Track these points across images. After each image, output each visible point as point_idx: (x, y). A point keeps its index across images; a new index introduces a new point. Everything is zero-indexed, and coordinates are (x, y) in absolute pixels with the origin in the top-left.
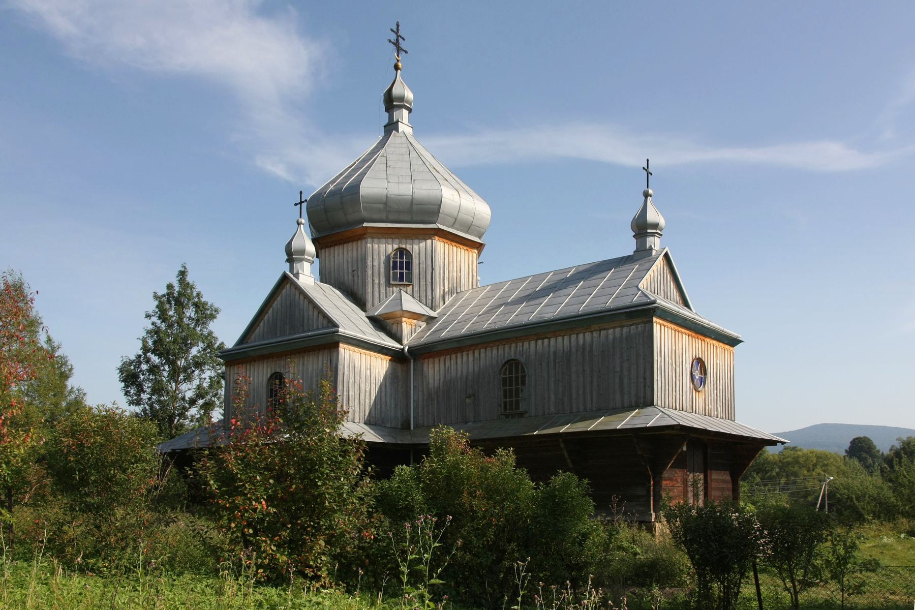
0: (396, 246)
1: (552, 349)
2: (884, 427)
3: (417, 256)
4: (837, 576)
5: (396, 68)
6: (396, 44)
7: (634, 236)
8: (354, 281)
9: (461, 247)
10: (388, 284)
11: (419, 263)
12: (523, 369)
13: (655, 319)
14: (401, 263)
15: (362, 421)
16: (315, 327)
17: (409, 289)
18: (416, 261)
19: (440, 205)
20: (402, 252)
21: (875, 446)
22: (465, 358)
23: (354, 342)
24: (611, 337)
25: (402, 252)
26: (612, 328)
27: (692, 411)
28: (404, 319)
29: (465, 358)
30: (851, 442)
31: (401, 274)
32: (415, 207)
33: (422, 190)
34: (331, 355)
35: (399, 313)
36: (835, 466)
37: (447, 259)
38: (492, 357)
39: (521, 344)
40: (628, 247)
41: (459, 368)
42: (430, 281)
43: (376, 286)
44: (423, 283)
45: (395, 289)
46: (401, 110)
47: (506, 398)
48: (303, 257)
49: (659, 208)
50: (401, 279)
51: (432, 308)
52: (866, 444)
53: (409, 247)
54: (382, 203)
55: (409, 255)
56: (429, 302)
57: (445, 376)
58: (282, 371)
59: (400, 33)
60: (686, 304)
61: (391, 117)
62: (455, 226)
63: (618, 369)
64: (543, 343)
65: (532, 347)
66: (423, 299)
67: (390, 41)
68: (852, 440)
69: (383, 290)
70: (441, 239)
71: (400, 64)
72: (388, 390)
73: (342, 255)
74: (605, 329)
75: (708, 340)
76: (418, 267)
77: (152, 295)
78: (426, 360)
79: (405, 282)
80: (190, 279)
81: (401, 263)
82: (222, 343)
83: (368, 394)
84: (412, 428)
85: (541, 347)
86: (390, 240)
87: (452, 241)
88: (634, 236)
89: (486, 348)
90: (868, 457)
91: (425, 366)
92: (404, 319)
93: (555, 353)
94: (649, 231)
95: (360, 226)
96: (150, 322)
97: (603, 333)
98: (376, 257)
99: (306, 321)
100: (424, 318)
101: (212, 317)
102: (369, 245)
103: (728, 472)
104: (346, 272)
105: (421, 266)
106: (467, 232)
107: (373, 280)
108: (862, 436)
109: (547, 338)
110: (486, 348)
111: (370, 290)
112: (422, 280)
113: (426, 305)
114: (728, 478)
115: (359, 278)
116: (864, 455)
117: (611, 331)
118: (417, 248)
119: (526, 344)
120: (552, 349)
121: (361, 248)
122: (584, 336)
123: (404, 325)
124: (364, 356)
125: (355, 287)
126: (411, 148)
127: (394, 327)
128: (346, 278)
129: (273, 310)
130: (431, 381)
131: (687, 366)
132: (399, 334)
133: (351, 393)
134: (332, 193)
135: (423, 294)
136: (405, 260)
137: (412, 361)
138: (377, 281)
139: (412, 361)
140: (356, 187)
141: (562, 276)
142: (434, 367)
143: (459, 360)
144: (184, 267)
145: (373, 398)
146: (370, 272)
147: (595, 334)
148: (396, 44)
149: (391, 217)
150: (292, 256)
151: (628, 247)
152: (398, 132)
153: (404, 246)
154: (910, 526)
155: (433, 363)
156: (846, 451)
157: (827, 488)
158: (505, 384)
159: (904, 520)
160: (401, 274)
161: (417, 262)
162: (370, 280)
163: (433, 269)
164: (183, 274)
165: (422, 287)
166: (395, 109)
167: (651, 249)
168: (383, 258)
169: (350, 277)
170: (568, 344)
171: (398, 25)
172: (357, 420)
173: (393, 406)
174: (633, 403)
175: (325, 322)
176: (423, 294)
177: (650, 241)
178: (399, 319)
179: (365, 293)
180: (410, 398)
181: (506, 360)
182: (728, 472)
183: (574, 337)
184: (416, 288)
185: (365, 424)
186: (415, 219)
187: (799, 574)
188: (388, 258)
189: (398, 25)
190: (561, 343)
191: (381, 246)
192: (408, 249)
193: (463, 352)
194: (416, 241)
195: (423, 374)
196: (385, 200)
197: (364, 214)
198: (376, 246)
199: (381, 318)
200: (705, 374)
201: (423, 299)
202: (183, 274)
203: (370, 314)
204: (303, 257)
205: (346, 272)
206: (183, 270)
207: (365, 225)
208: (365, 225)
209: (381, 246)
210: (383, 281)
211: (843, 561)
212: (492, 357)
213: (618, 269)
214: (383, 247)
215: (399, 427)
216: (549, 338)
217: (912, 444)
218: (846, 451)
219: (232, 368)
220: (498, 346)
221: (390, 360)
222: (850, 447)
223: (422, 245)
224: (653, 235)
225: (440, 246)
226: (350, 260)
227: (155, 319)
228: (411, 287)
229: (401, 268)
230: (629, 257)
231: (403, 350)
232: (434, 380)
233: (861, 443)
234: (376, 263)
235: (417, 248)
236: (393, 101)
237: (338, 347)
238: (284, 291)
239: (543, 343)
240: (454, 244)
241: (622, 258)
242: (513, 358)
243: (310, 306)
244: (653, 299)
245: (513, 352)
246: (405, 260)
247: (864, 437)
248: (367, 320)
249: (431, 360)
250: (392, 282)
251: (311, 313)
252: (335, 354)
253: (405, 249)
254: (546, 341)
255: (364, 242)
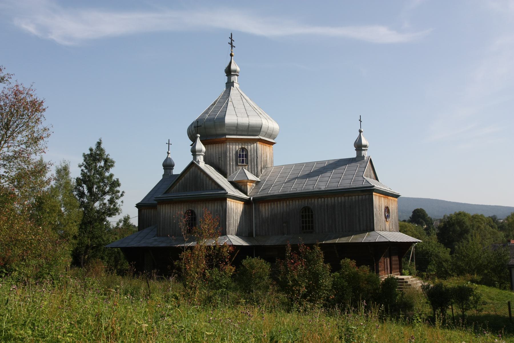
0: (240, 147)
1: (326, 203)
2: (429, 199)
3: (250, 151)
4: (475, 307)
5: (231, 55)
6: (231, 44)
7: (355, 150)
8: (219, 162)
9: (267, 145)
10: (237, 165)
11: (251, 155)
12: (312, 212)
13: (374, 193)
14: (243, 155)
15: (235, 234)
16: (210, 189)
17: (247, 167)
18: (249, 154)
19: (261, 128)
20: (243, 149)
21: (427, 214)
22: (281, 204)
23: (232, 197)
24: (354, 200)
25: (243, 149)
26: (354, 196)
27: (386, 230)
28: (248, 183)
29: (281, 204)
30: (413, 212)
31: (243, 160)
32: (250, 129)
33: (253, 120)
34: (222, 204)
35: (246, 181)
36: (410, 231)
37: (262, 152)
38: (296, 205)
39: (310, 200)
40: (353, 154)
41: (279, 208)
42: (256, 163)
43: (231, 166)
44: (253, 164)
45: (240, 167)
46: (234, 76)
47: (304, 224)
48: (201, 153)
49: (366, 139)
50: (243, 162)
51: (257, 176)
52: (422, 213)
53: (246, 147)
54: (235, 127)
55: (247, 151)
56: (256, 173)
57: (271, 212)
58: (193, 209)
59: (233, 39)
60: (377, 179)
61: (229, 79)
62: (266, 136)
63: (358, 214)
64: (321, 200)
65: (316, 202)
66: (253, 172)
67: (235, 47)
68: (413, 210)
69: (234, 168)
70: (260, 143)
71: (233, 54)
72: (243, 218)
73: (216, 149)
74: (351, 196)
75: (389, 197)
76: (250, 156)
77: (82, 154)
78: (261, 204)
79: (245, 164)
80: (102, 146)
81: (243, 155)
82: (118, 179)
83: (236, 221)
84: (254, 236)
85: (320, 202)
86: (237, 144)
87: (264, 143)
88: (355, 150)
89: (292, 200)
90: (423, 221)
91: (260, 207)
92: (248, 183)
93: (327, 205)
94: (363, 148)
95: (224, 137)
96: (81, 169)
97: (350, 197)
98: (231, 152)
99: (205, 185)
100: (255, 182)
101: (112, 166)
102: (228, 146)
103: (397, 256)
104: (215, 158)
105: (252, 156)
106: (270, 138)
107: (230, 163)
108: (419, 208)
109: (323, 198)
110: (292, 200)
111: (228, 168)
112: (252, 163)
113: (254, 175)
114: (398, 259)
115: (223, 161)
116: (421, 220)
117: (354, 197)
118: (250, 147)
119: (313, 200)
120: (326, 203)
121: (224, 147)
122: (341, 198)
123: (248, 186)
124: (238, 204)
125: (220, 166)
126: (242, 97)
127: (243, 187)
128: (215, 161)
129: (185, 178)
130: (264, 214)
131: (383, 211)
132: (245, 190)
133: (231, 221)
134: (209, 120)
135: (253, 170)
136: (244, 153)
137: (254, 204)
138: (232, 164)
139: (254, 204)
140: (223, 118)
141: (322, 165)
142: (265, 207)
143: (279, 205)
144: (101, 140)
145: (238, 223)
146: (228, 159)
147: (346, 198)
148: (231, 44)
149: (239, 133)
150: (194, 152)
151: (353, 154)
152: (234, 87)
153: (244, 147)
154: (471, 278)
155: (265, 206)
156: (410, 217)
157: (414, 249)
158: (303, 218)
159: (468, 275)
160: (243, 160)
161: (250, 154)
162: (228, 163)
163: (257, 158)
164: (99, 144)
165: (252, 166)
166: (232, 76)
167: (364, 157)
168: (234, 152)
169: (217, 160)
170: (334, 201)
171: (232, 35)
172: (233, 234)
173: (245, 225)
174: (365, 230)
175: (216, 187)
176: (253, 170)
177: (363, 152)
178: (246, 183)
179: (226, 170)
180: (253, 221)
181: (303, 206)
182: (397, 256)
183: (336, 198)
184: (250, 167)
185: (236, 235)
186: (249, 134)
187: (464, 306)
188: (237, 152)
189: (232, 35)
190: (330, 201)
191: (233, 146)
192: (246, 148)
193: (280, 201)
194: (249, 144)
195: (259, 211)
196: (236, 125)
197: (226, 131)
198: (231, 146)
199: (236, 182)
200: (389, 213)
201: (253, 172)
202: (99, 144)
203: (230, 180)
204: (201, 153)
205: (215, 158)
206: (100, 141)
207: (227, 137)
208: (227, 137)
209: (233, 146)
210: (234, 164)
211: (476, 302)
212: (296, 205)
213: (349, 165)
214: (234, 147)
215: (247, 235)
216: (324, 198)
217: (453, 219)
218: (410, 217)
219: (161, 206)
220: (299, 200)
221: (244, 204)
222: (412, 215)
223: (252, 146)
224: (364, 150)
225: (259, 145)
226: (217, 152)
227: (83, 168)
228: (247, 166)
229: (243, 157)
230: (353, 159)
231: (250, 199)
232: (265, 214)
233: (419, 213)
234: (231, 155)
235: (250, 147)
236: (231, 72)
237: (226, 200)
238: (191, 170)
239: (321, 200)
240: (264, 144)
241: (350, 159)
242: (306, 206)
243: (207, 178)
244: (373, 185)
245: (306, 203)
246: (244, 153)
247: (421, 209)
248: (229, 183)
249: (263, 204)
250: (239, 164)
251: (208, 182)
252: (224, 204)
253: (245, 148)
254: (323, 199)
255: (225, 144)
